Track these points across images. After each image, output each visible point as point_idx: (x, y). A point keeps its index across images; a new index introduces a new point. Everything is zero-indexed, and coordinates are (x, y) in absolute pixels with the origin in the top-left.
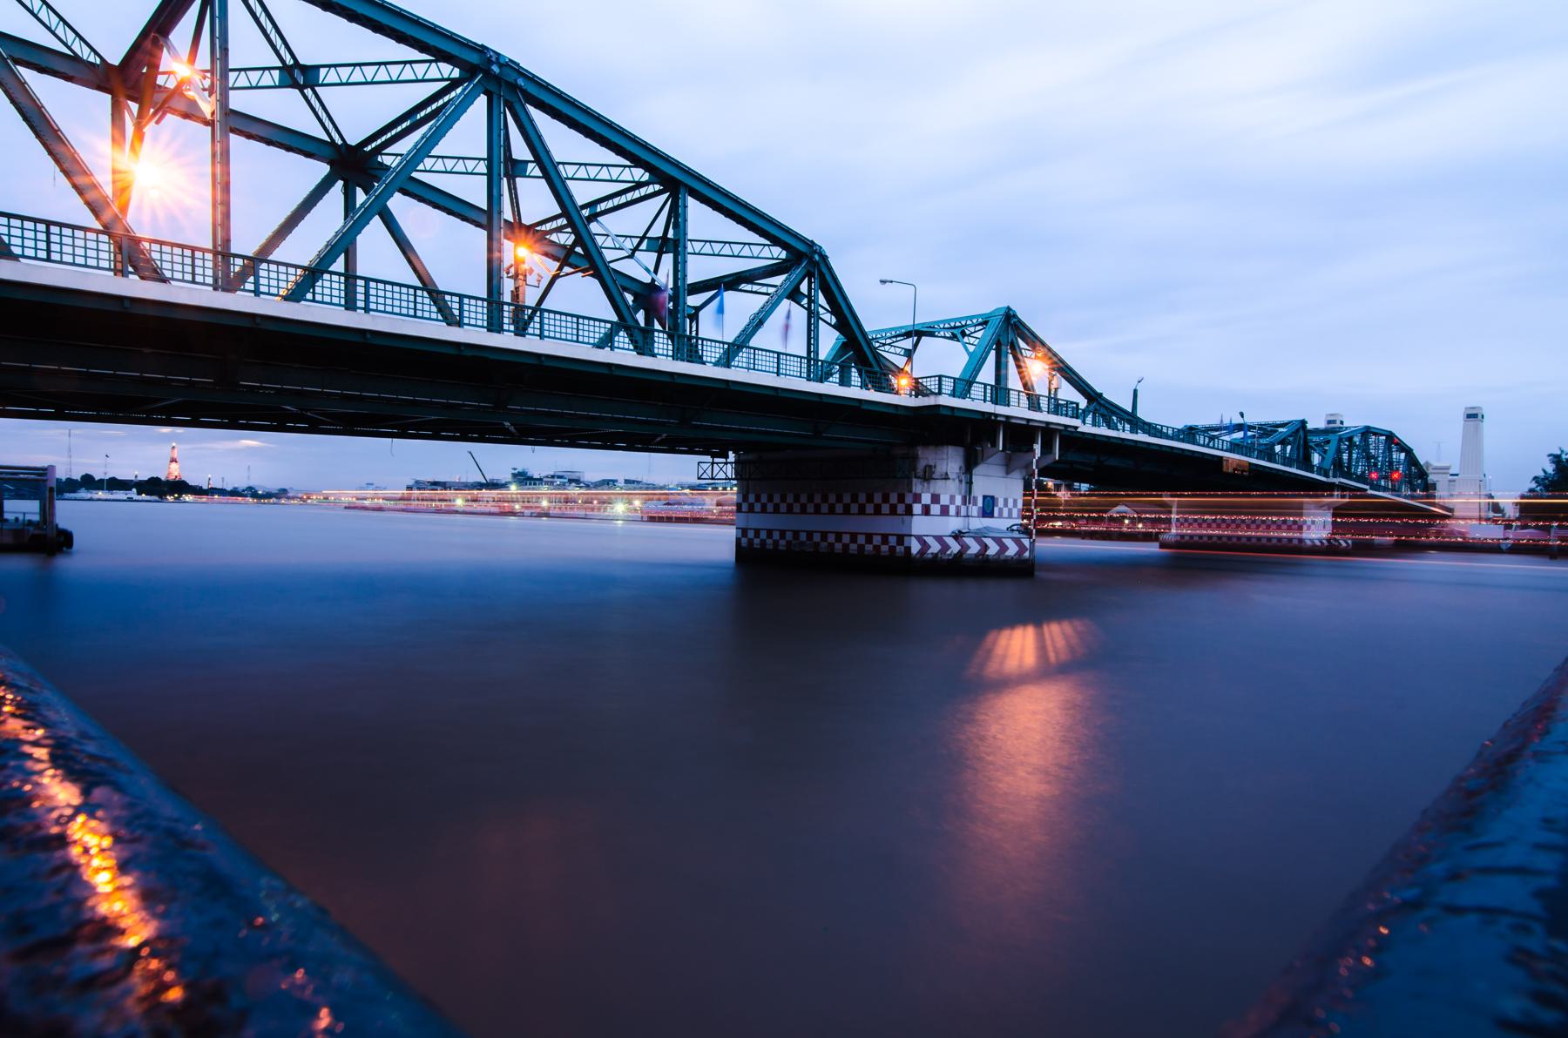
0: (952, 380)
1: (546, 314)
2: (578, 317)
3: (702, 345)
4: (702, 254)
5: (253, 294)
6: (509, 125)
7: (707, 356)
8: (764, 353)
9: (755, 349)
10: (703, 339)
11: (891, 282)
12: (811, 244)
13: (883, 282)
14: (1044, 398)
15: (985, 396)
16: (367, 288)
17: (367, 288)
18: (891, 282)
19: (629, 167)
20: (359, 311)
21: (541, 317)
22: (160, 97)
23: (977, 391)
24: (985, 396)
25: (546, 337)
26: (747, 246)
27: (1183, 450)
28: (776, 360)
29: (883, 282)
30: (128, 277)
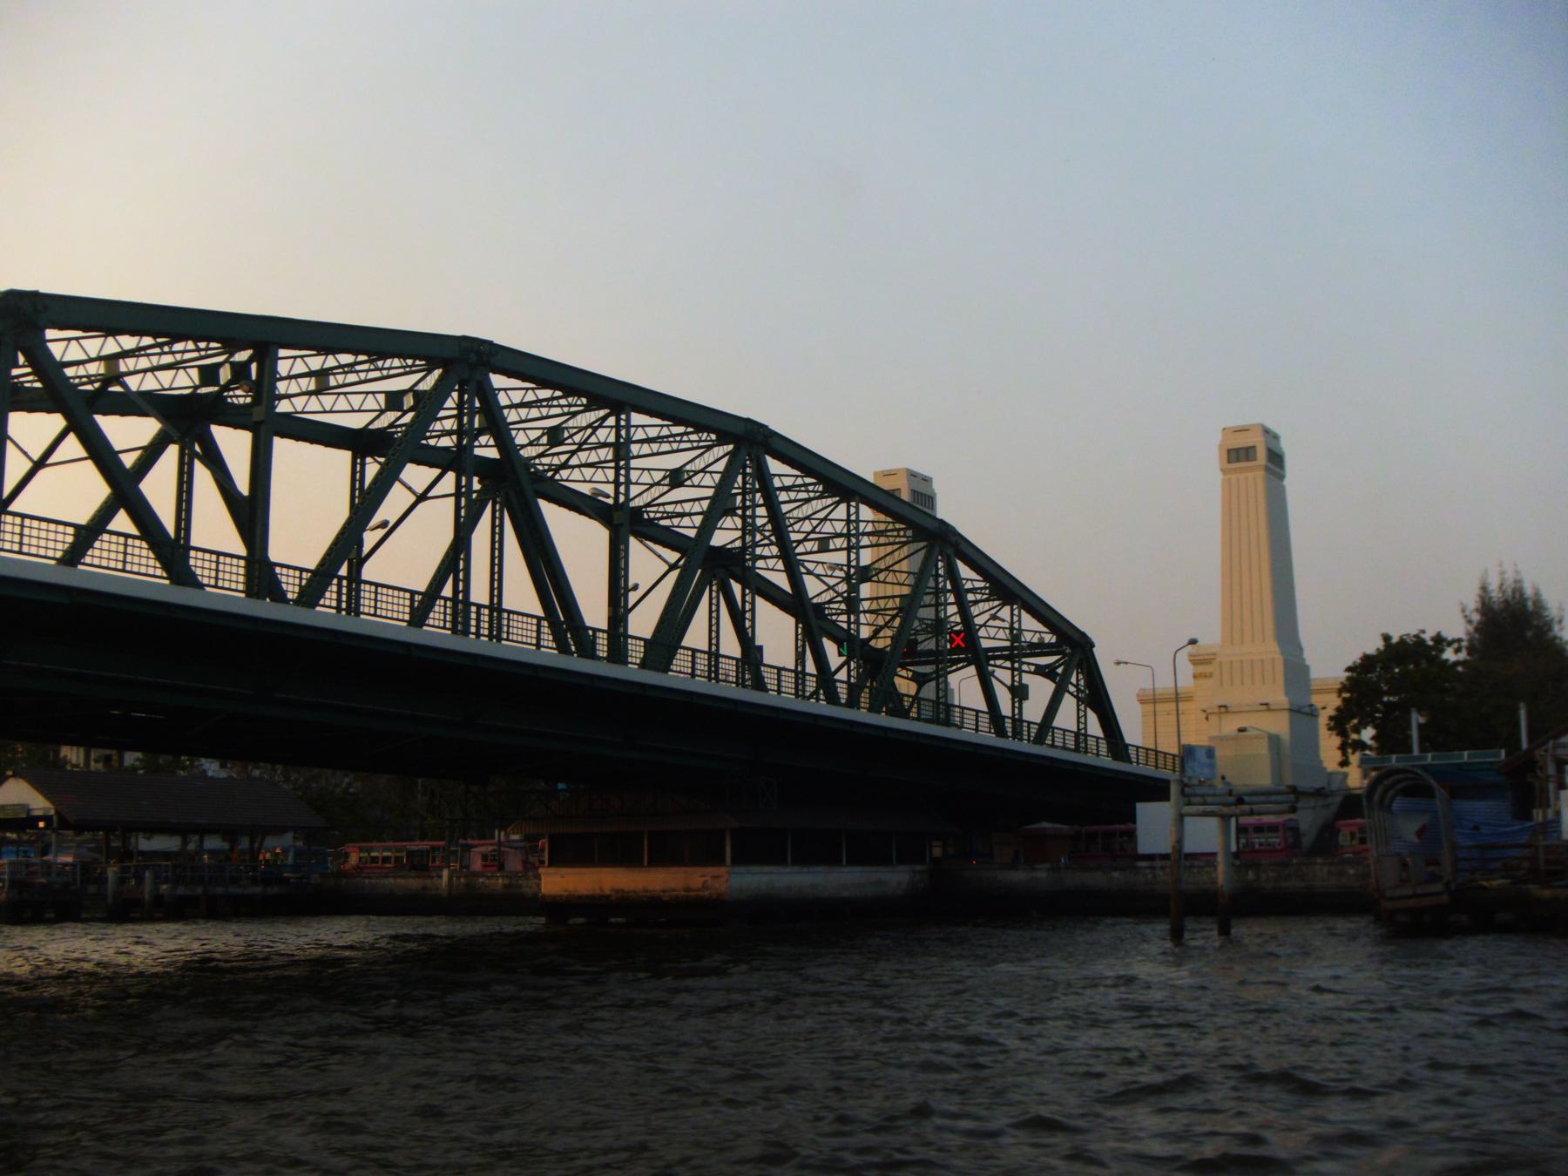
0: (776, 671)
1: (922, 702)
2: (219, 554)
3: (509, 619)
4: (777, 570)
5: (689, 676)
6: (692, 452)
7: (632, 656)
8: (396, 593)
9: (23, 516)
10: (510, 612)
11: (1127, 663)
12: (1083, 635)
13: (1118, 663)
14: (842, 685)
15: (1174, 767)
16: (1029, 727)
17: (1029, 727)
18: (1127, 663)
19: (533, 389)
20: (862, 710)
21: (919, 705)
22: (397, 443)
23: (681, 662)
24: (1174, 767)
25: (722, 681)
26: (588, 479)
27: (917, 735)
28: (535, 628)
29: (1118, 663)
30: (468, 636)
